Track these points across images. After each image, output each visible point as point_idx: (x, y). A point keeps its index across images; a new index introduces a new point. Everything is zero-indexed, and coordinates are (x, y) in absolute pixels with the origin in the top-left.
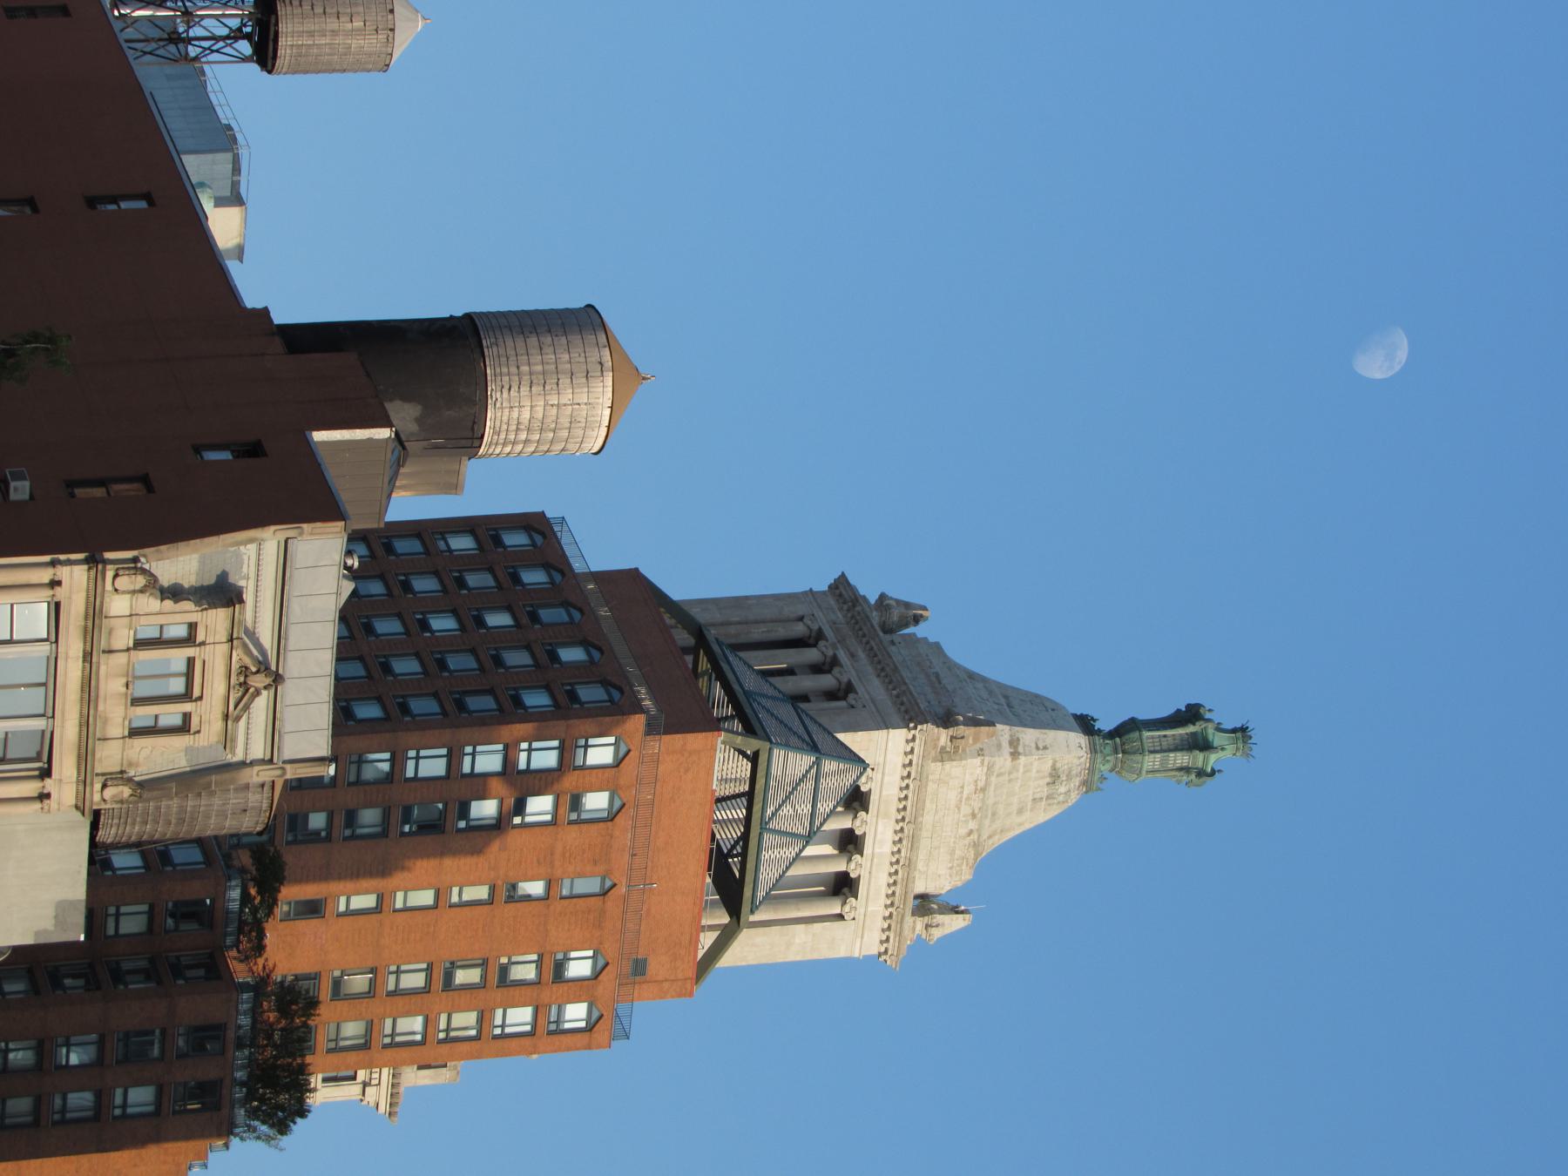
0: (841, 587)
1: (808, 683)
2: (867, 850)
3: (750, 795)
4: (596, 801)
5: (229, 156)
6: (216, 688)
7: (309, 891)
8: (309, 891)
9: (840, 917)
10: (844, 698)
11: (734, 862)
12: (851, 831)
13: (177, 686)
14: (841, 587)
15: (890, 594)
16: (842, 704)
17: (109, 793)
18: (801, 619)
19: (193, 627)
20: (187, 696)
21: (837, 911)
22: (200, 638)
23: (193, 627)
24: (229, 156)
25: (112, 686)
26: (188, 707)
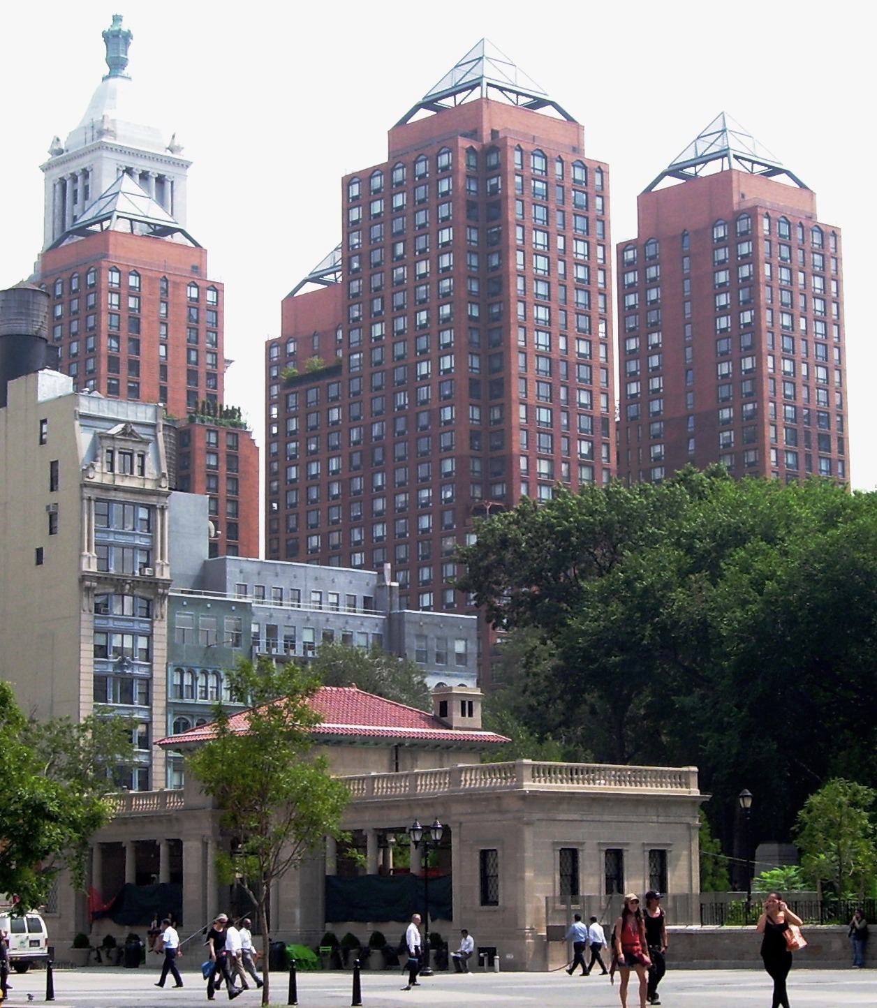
0: (46, 168)
1: (80, 186)
2: (164, 173)
3: (131, 220)
4: (133, 281)
5: (480, 727)
6: (129, 445)
7: (623, 617)
8: (623, 617)
9: (172, 182)
10: (88, 172)
11: (158, 228)
12: (156, 178)
13: (128, 457)
14: (46, 168)
15: (49, 148)
16: (90, 174)
17: (163, 485)
18: (55, 185)
19: (108, 451)
20: (131, 455)
21: (170, 184)
22: (111, 449)
23: (108, 451)
24: (480, 727)
25: (127, 483)
26: (136, 455)
